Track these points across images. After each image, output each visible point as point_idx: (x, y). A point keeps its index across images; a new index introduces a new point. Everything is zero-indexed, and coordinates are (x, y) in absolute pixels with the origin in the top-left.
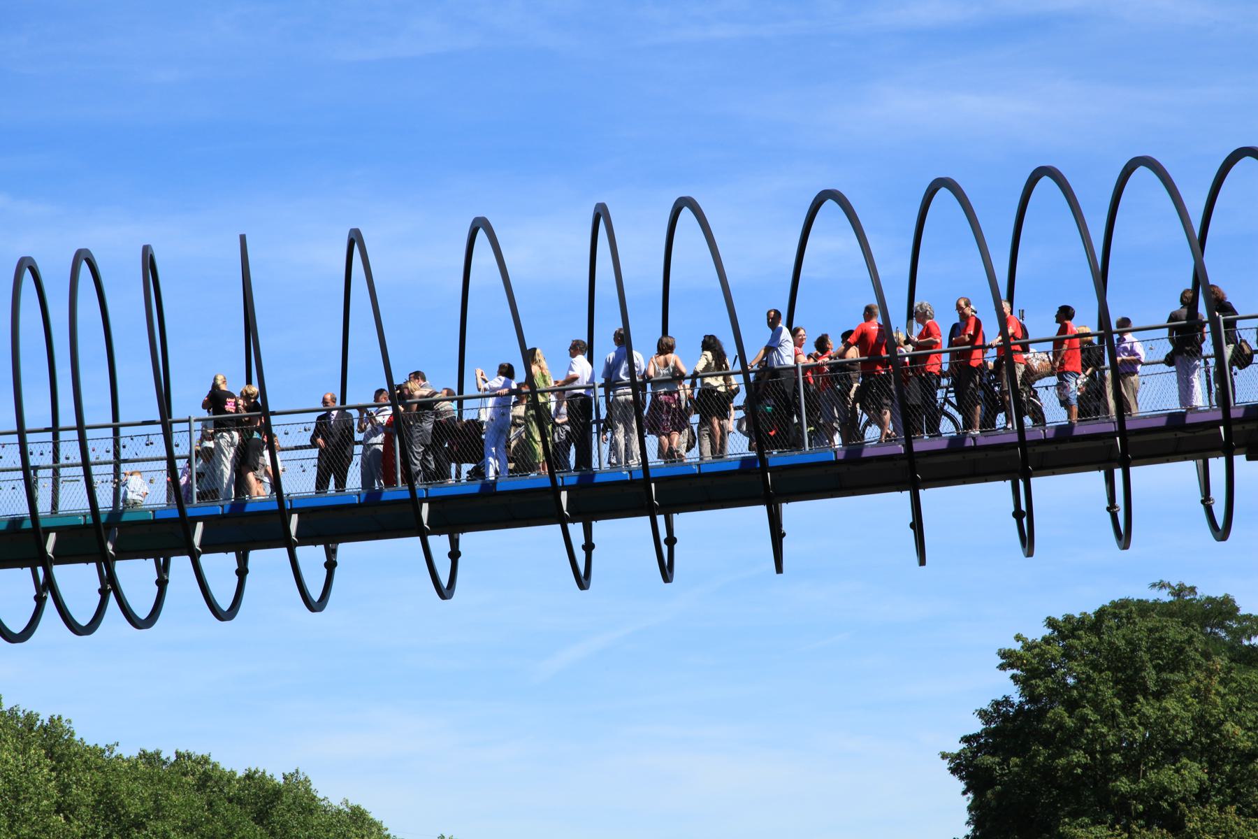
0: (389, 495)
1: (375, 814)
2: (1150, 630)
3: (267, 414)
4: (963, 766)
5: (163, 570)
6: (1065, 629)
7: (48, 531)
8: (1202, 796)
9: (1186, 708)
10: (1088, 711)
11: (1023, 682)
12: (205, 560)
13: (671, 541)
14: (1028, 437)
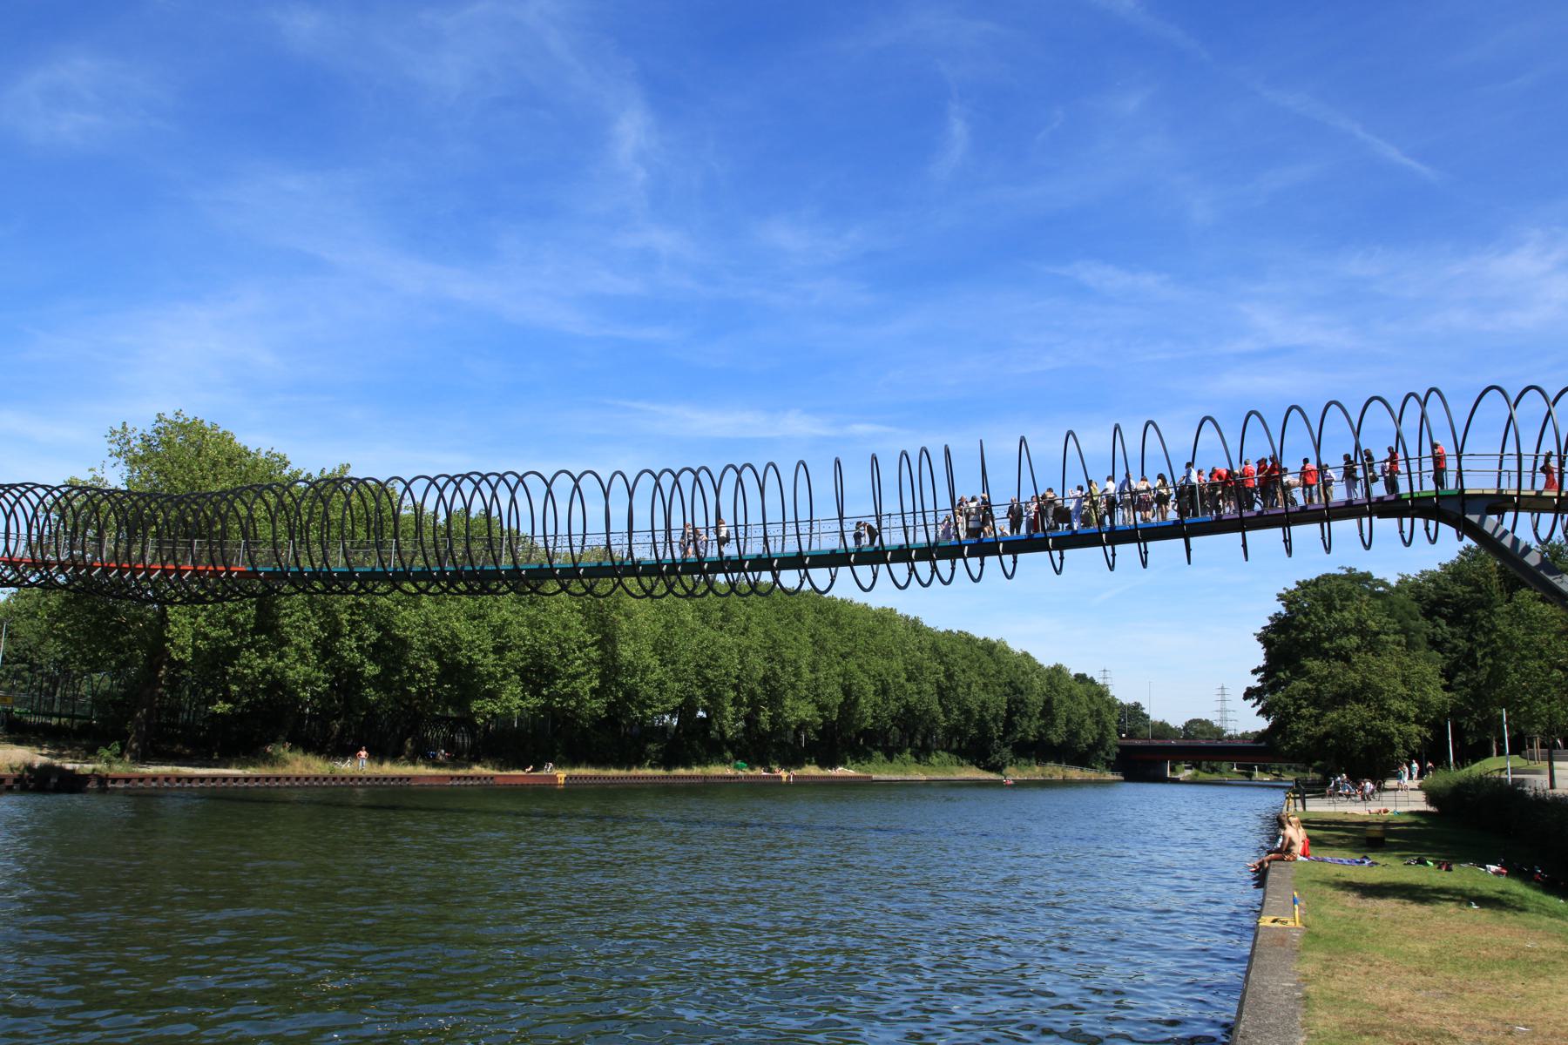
0: (1036, 536)
1: (1032, 655)
2: (1338, 585)
3: (991, 506)
4: (1264, 638)
5: (953, 564)
6: (1303, 586)
7: (965, 545)
8: (1358, 649)
9: (1352, 615)
10: (1312, 617)
11: (1286, 606)
12: (969, 560)
13: (1146, 552)
14: (1289, 510)
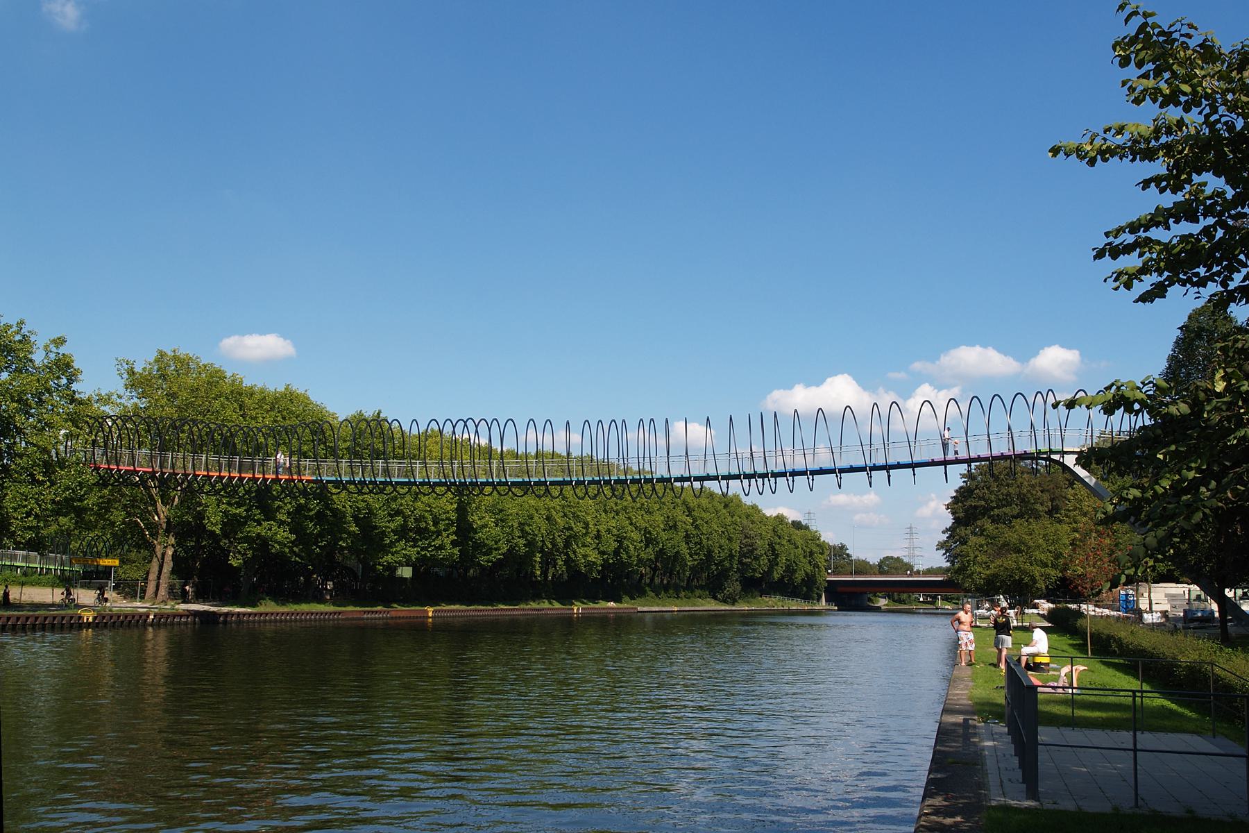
13: (871, 477)
